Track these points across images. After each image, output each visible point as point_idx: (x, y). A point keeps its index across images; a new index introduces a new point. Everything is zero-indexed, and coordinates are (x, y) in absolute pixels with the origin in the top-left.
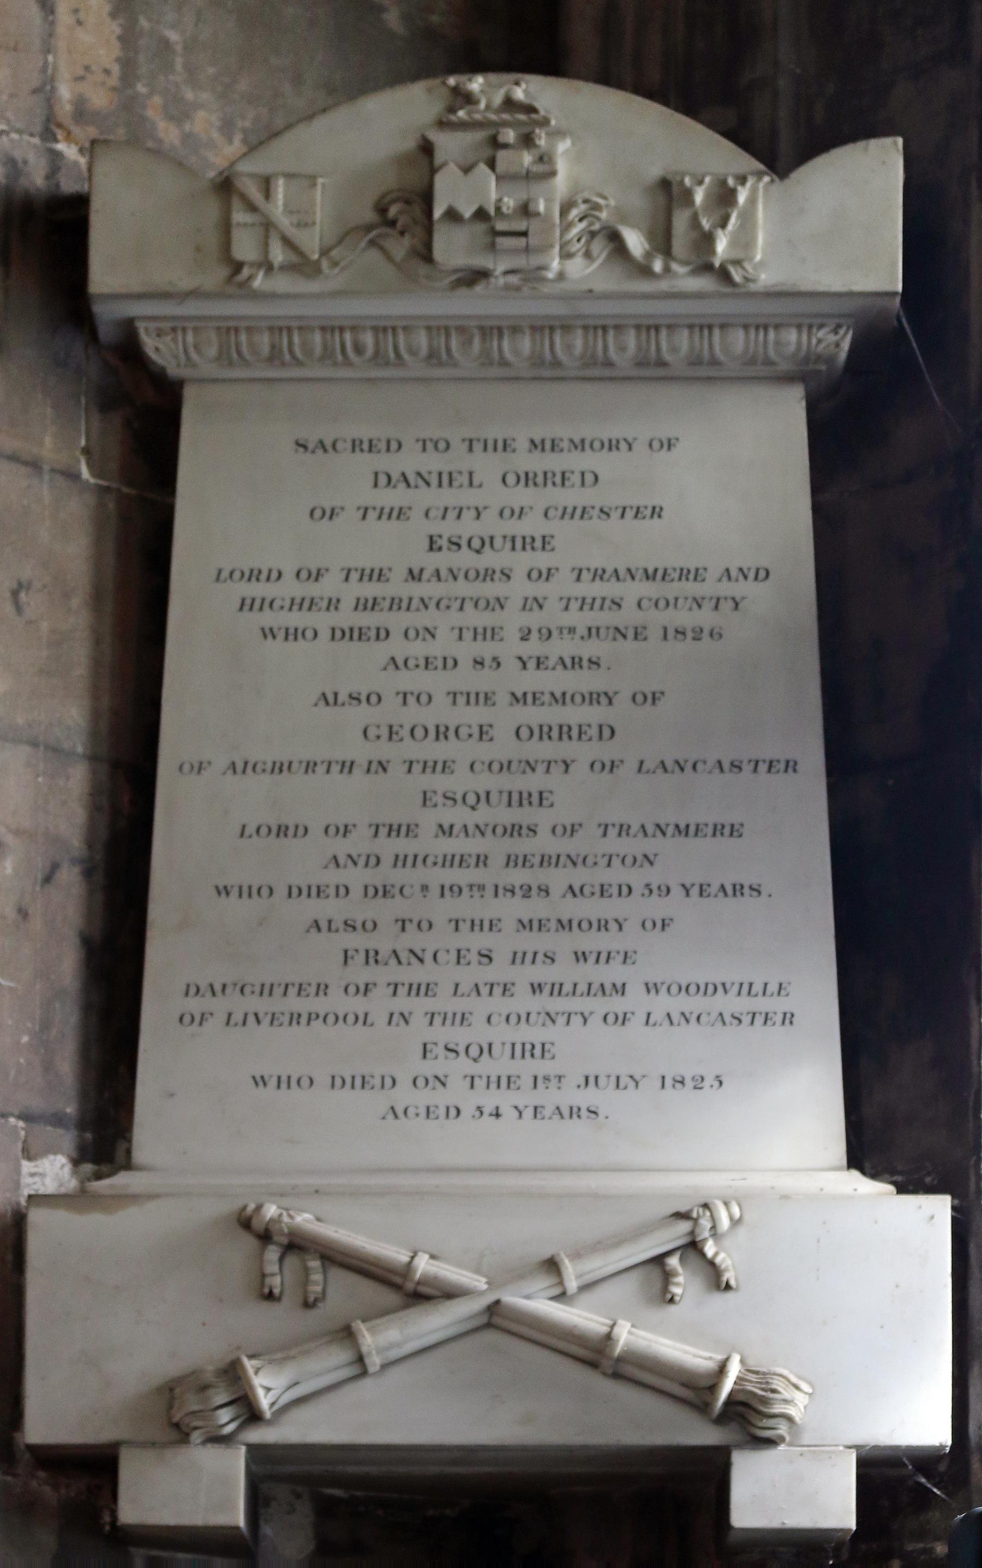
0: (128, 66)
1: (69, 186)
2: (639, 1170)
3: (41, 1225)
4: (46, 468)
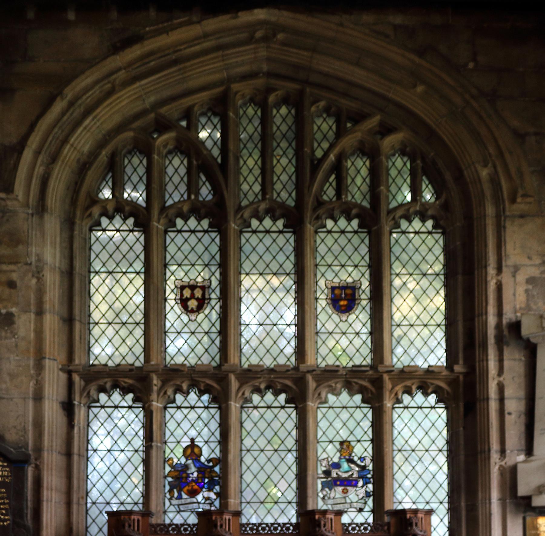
0: (528, 300)
1: (519, 319)
2: (69, 504)
3: (520, 467)
4: (499, 278)
